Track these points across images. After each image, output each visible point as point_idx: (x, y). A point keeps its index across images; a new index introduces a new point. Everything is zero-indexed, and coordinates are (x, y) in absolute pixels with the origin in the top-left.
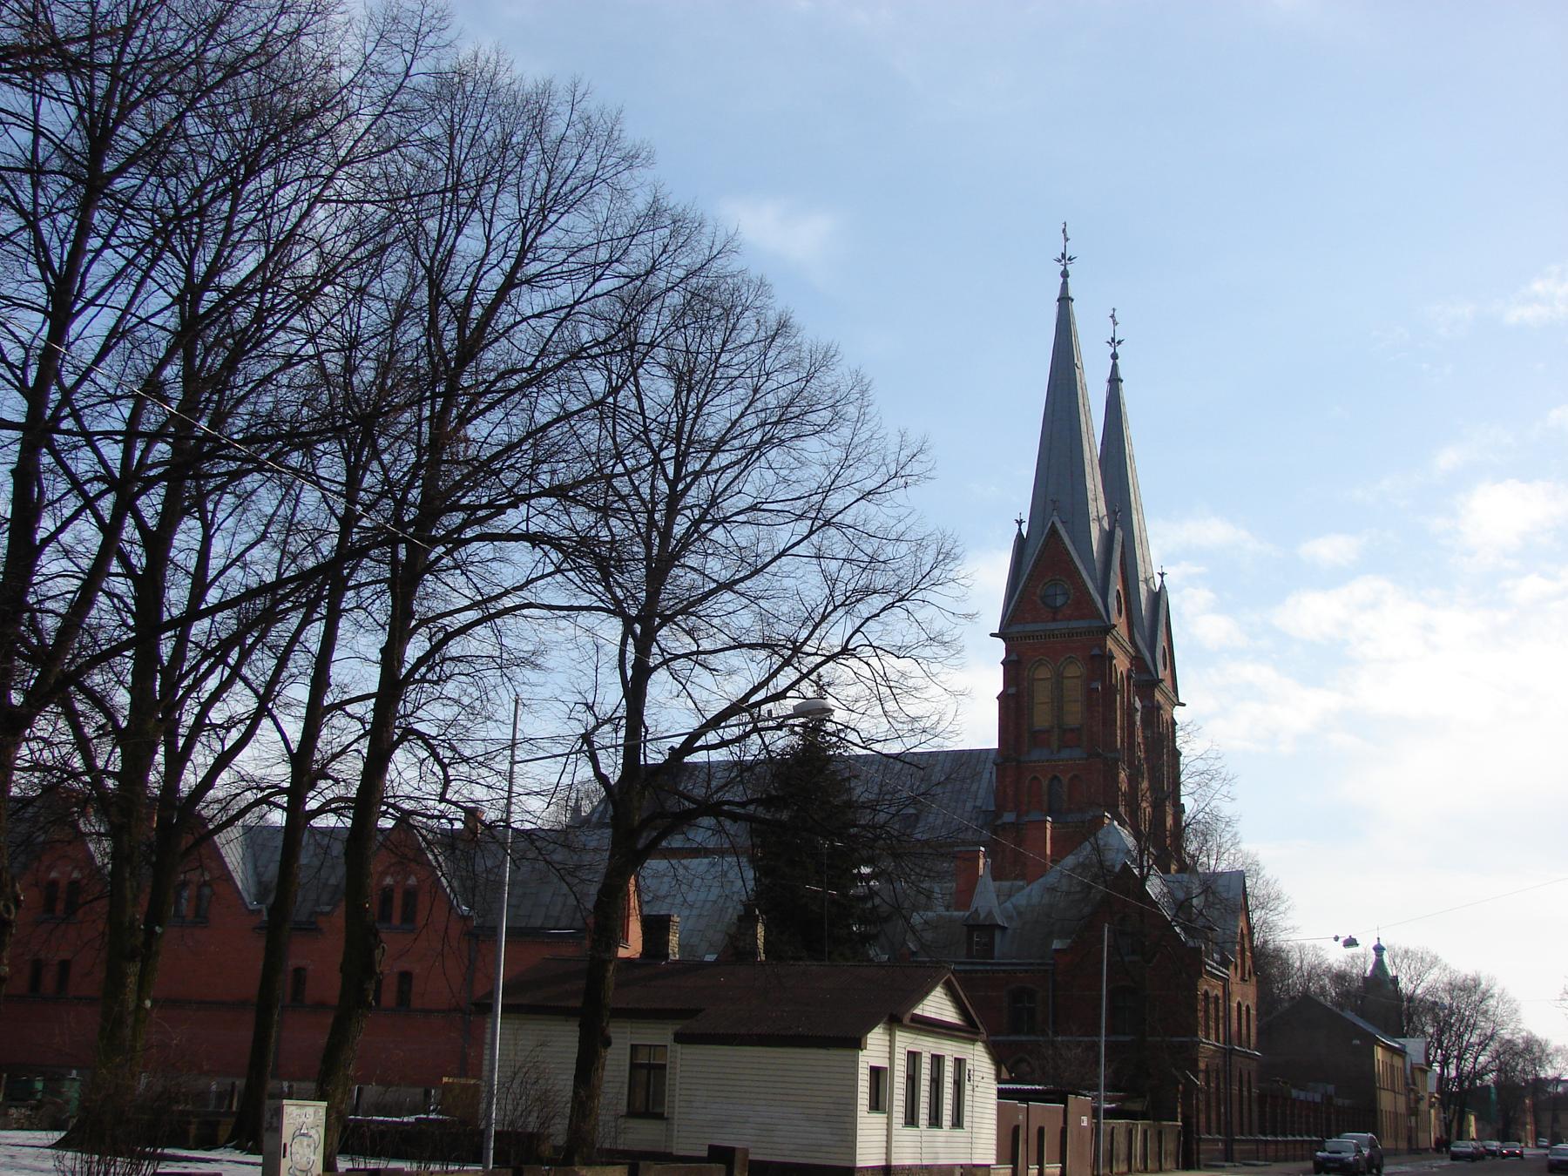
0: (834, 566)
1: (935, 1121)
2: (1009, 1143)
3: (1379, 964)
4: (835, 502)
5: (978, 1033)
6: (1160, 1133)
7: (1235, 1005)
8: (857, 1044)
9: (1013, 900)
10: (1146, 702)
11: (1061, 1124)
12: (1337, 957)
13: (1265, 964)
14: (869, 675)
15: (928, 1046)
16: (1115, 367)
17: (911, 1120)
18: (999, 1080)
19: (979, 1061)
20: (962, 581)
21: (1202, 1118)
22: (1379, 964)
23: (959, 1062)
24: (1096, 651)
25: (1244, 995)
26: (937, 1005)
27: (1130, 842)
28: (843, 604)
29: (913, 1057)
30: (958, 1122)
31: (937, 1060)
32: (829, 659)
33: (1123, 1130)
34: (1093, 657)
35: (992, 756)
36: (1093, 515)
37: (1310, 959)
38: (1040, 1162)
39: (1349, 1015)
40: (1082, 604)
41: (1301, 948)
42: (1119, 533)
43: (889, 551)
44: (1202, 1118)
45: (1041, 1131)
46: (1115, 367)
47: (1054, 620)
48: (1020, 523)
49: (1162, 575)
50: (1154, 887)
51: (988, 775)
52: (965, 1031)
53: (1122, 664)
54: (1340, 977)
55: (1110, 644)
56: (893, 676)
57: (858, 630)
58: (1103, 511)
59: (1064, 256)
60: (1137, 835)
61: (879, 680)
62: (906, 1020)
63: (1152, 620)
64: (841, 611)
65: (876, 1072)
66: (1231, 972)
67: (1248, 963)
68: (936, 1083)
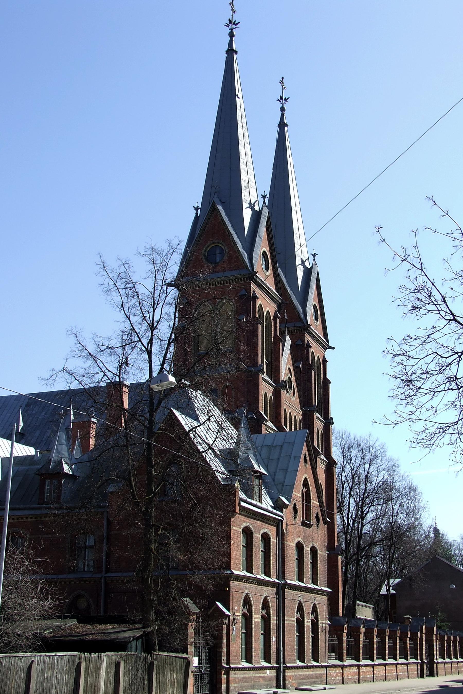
16: (282, 116)
24: (243, 292)
34: (241, 297)
46: (282, 116)
48: (197, 209)
49: (314, 255)
59: (281, 98)
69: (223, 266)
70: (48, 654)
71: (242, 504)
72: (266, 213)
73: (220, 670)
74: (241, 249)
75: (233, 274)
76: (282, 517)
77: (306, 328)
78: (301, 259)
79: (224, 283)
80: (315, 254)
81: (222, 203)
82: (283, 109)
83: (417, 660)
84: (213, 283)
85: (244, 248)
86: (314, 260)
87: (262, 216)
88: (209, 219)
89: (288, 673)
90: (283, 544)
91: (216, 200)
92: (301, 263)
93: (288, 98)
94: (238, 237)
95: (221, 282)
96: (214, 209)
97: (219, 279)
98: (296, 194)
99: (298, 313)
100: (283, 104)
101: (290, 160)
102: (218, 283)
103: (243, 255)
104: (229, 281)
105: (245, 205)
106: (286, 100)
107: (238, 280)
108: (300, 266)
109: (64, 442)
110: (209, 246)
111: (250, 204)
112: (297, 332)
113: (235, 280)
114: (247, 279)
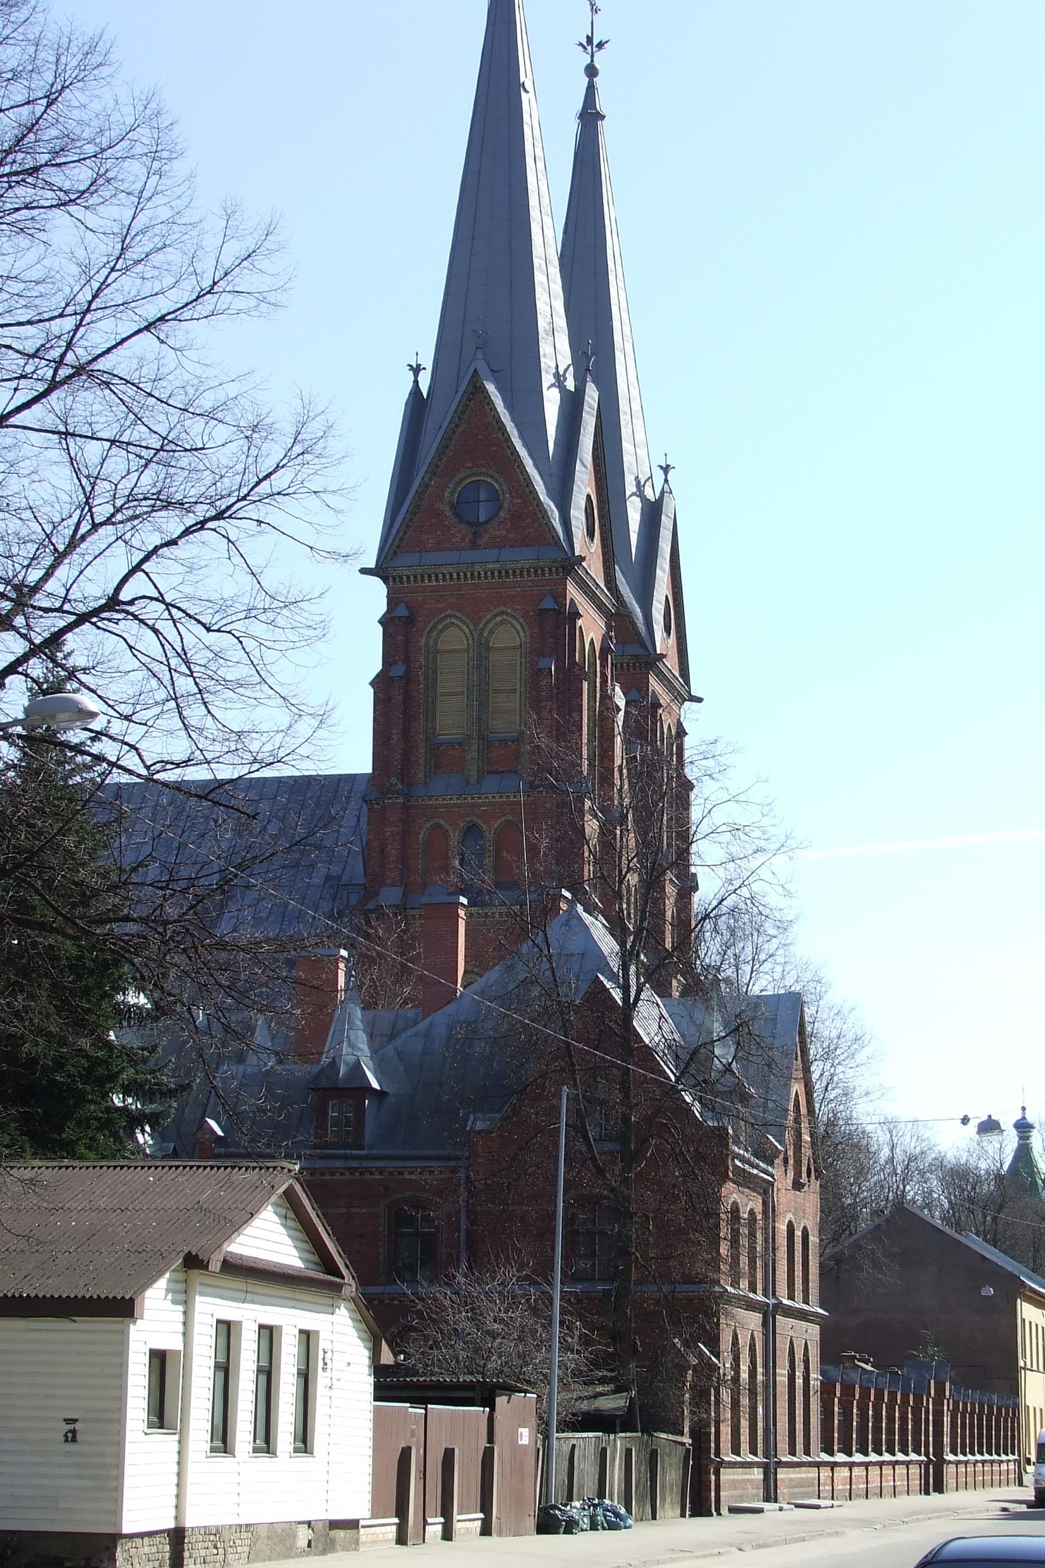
0: (93, 451)
1: (266, 1443)
2: (301, 1396)
3: (1024, 1153)
4: (98, 335)
5: (338, 1288)
6: (654, 1454)
7: (782, 1227)
8: (125, 1309)
9: (398, 1042)
10: (634, 695)
11: (484, 1443)
12: (955, 1144)
13: (833, 1154)
14: (156, 651)
15: (250, 1314)
16: (591, 90)
17: (222, 1440)
18: (558, 1533)
19: (343, 1340)
20: (334, 501)
21: (726, 1430)
22: (1024, 1153)
23: (307, 1337)
24: (548, 603)
25: (799, 1209)
26: (268, 1238)
27: (608, 945)
28: (108, 521)
29: (227, 1330)
30: (304, 1442)
31: (269, 1334)
32: (82, 619)
33: (591, 1449)
34: (542, 613)
35: (361, 787)
36: (547, 363)
37: (908, 1143)
38: (446, 1512)
39: (975, 1242)
40: (527, 523)
41: (890, 1125)
42: (592, 395)
43: (196, 430)
44: (726, 1430)
45: (449, 1456)
46: (591, 90)
47: (475, 546)
48: (416, 370)
49: (666, 469)
50: (652, 1022)
51: (352, 817)
52: (315, 1283)
53: (592, 627)
54: (958, 1176)
55: (572, 591)
56: (199, 657)
57: (137, 568)
58: (565, 359)
59: (590, 40)
60: (617, 928)
61: (174, 662)
62: (215, 1265)
63: (643, 549)
64: (107, 533)
65: (159, 1359)
66: (777, 1171)
67: (807, 1152)
68: (267, 1373)
69: (497, 533)
70: (585, 1435)
71: (737, 1163)
72: (593, 399)
73: (707, 1466)
74: (543, 496)
75: (522, 557)
76: (772, 1176)
77: (651, 661)
78: (637, 478)
79: (500, 577)
80: (668, 466)
81: (496, 375)
82: (591, 71)
83: (920, 1455)
84: (472, 574)
85: (550, 495)
86: (666, 481)
87: (586, 407)
88: (463, 412)
89: (782, 1474)
90: (774, 1228)
91: (481, 366)
92: (635, 490)
93: (607, 42)
94: (536, 465)
95: (493, 573)
96: (476, 388)
97: (490, 566)
98: (623, 305)
99: (633, 623)
100: (592, 56)
101: (611, 213)
102: (486, 573)
103: (549, 513)
104: (514, 572)
105: (547, 379)
106: (600, 45)
107: (536, 571)
108: (634, 498)
109: (359, 1023)
110: (463, 480)
111: (557, 375)
112: (629, 670)
113: (529, 571)
114: (557, 569)
